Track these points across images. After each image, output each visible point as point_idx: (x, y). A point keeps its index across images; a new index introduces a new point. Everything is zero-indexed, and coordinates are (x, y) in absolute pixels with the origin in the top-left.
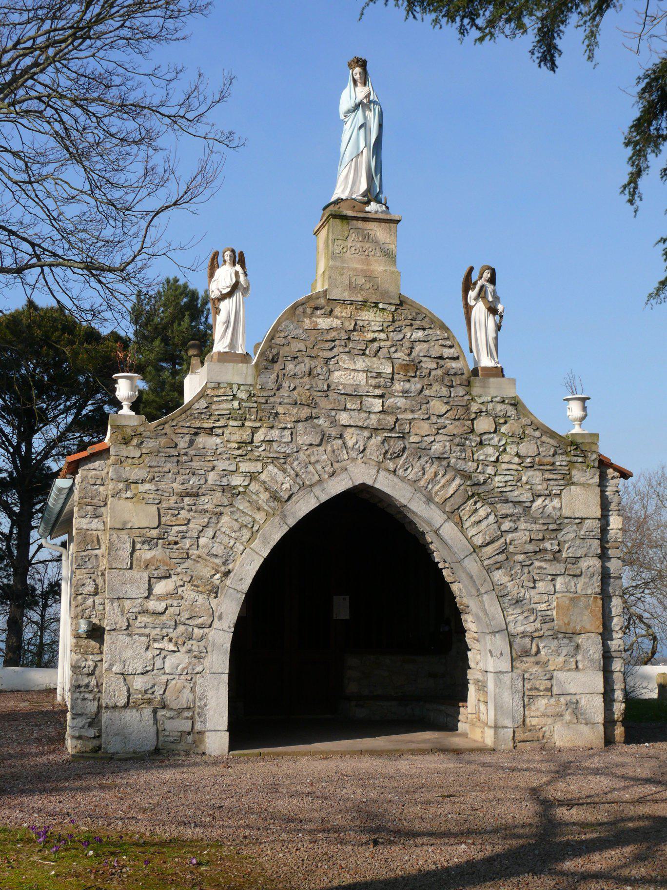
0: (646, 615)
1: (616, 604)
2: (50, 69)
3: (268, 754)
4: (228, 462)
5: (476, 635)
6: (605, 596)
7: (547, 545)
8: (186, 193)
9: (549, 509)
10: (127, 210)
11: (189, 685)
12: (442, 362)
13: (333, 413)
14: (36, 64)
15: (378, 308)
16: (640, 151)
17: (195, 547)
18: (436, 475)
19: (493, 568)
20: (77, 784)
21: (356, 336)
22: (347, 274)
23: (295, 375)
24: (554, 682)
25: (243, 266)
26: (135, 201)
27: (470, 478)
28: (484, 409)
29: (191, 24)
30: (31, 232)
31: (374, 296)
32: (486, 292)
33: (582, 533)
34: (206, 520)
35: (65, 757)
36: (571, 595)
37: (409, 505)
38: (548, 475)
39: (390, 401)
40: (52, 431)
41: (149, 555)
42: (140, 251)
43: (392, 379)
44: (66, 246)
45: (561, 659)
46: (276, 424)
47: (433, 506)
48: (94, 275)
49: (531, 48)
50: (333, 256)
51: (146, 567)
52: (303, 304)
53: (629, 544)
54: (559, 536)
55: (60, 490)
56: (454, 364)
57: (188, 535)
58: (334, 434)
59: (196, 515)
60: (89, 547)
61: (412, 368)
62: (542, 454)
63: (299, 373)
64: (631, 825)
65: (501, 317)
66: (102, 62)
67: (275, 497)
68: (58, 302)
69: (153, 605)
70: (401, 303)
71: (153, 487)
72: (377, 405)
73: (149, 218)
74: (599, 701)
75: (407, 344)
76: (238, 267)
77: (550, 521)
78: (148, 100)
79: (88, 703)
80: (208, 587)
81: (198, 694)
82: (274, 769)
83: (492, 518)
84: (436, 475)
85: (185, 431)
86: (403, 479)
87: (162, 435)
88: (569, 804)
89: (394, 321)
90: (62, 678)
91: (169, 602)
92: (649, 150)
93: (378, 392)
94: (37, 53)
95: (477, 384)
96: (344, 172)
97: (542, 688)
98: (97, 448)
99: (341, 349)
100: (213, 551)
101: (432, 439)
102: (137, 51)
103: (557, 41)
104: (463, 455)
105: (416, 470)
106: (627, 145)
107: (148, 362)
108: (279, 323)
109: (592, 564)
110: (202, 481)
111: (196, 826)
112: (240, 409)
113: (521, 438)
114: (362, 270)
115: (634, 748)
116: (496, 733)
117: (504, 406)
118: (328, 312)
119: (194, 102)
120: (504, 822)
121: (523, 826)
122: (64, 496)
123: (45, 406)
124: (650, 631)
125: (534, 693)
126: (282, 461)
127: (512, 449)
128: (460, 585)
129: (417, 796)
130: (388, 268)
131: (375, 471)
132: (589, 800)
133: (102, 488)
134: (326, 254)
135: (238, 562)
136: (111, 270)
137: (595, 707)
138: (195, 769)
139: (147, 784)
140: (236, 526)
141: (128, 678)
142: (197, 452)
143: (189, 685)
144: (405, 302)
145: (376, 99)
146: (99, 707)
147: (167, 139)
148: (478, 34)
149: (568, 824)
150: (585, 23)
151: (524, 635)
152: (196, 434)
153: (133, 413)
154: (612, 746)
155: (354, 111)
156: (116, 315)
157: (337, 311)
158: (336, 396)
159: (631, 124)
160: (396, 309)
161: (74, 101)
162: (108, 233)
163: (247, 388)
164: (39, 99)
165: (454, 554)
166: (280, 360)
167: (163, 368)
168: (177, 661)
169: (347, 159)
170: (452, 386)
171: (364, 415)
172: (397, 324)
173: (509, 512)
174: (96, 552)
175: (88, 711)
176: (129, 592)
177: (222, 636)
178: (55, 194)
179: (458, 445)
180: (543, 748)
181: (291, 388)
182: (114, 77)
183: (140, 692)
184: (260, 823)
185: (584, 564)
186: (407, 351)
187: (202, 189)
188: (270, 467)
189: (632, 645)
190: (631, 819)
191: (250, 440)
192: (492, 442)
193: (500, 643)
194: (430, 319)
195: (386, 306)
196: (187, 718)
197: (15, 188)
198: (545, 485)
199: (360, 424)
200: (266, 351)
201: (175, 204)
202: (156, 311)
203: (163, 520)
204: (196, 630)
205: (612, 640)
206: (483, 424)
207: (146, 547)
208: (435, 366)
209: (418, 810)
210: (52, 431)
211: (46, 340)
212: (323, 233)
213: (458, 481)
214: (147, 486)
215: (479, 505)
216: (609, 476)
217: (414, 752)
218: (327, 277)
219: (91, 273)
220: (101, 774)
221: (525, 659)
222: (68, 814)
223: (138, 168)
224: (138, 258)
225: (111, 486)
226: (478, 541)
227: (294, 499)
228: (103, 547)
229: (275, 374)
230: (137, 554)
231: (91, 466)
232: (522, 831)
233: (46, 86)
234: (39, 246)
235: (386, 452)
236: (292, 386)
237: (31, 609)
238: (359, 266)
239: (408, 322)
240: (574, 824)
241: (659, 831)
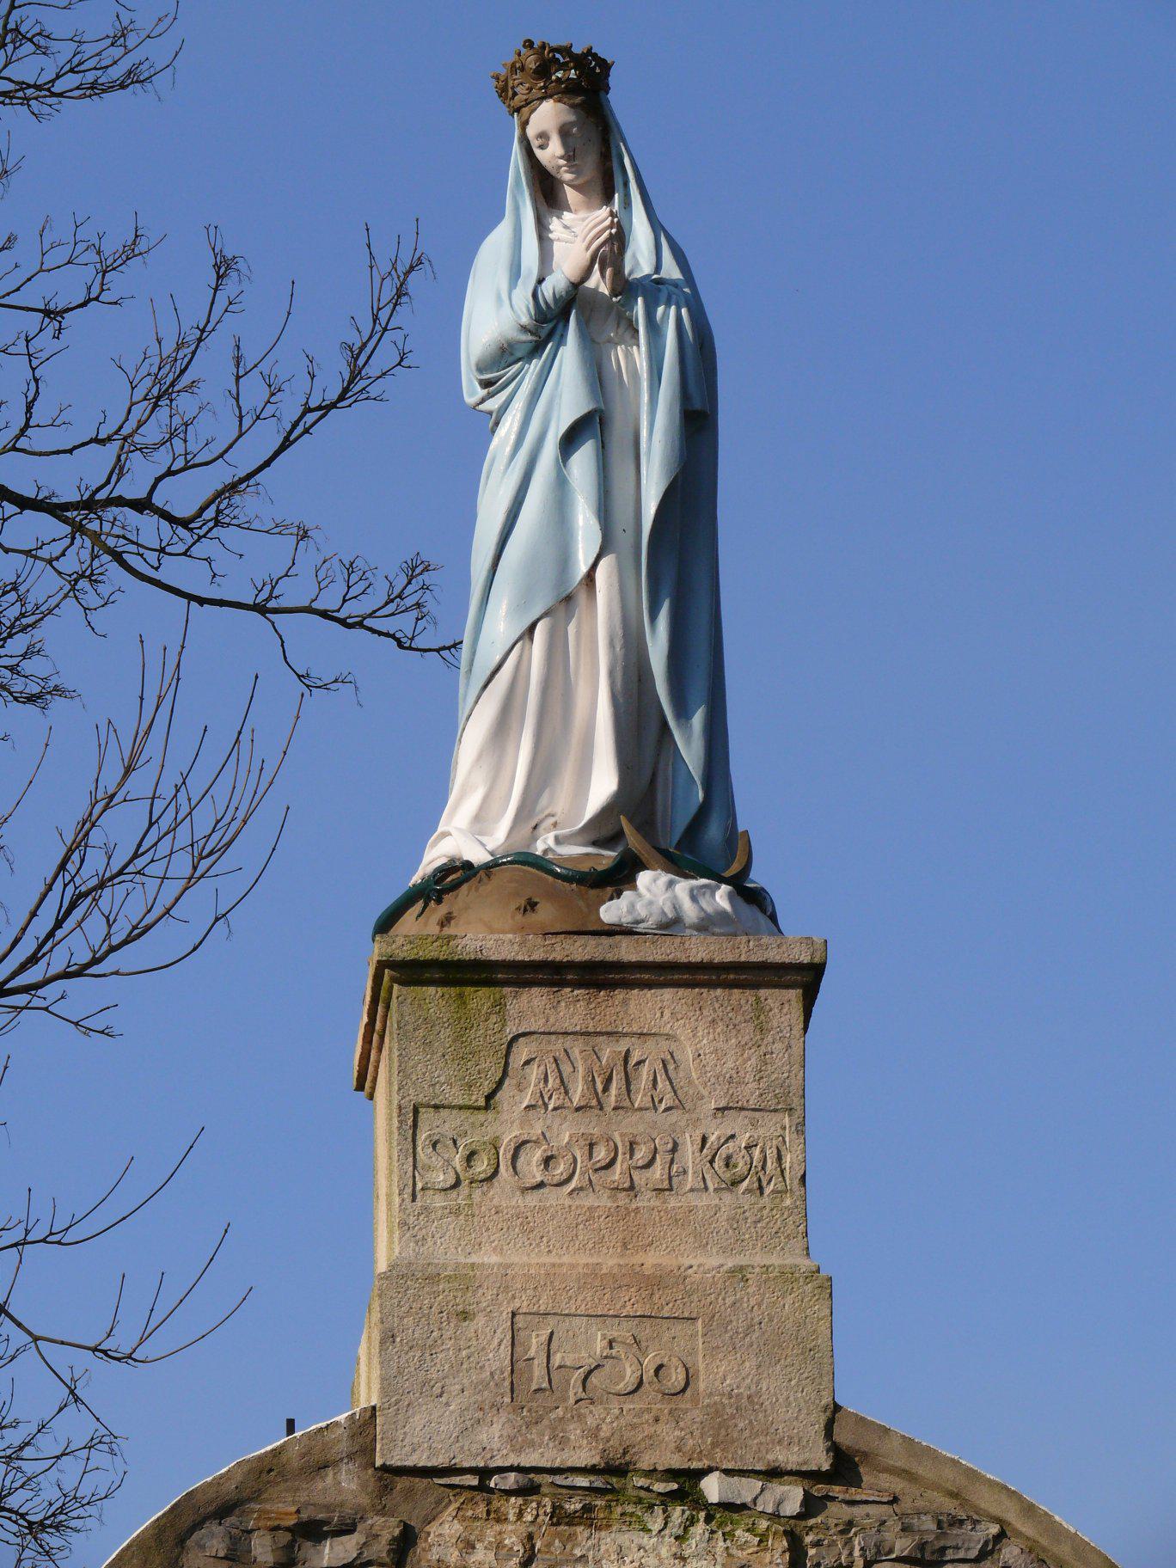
31: (669, 1433)
145: (671, 271)
155: (536, 349)
160: (811, 1506)
195: (746, 1490)
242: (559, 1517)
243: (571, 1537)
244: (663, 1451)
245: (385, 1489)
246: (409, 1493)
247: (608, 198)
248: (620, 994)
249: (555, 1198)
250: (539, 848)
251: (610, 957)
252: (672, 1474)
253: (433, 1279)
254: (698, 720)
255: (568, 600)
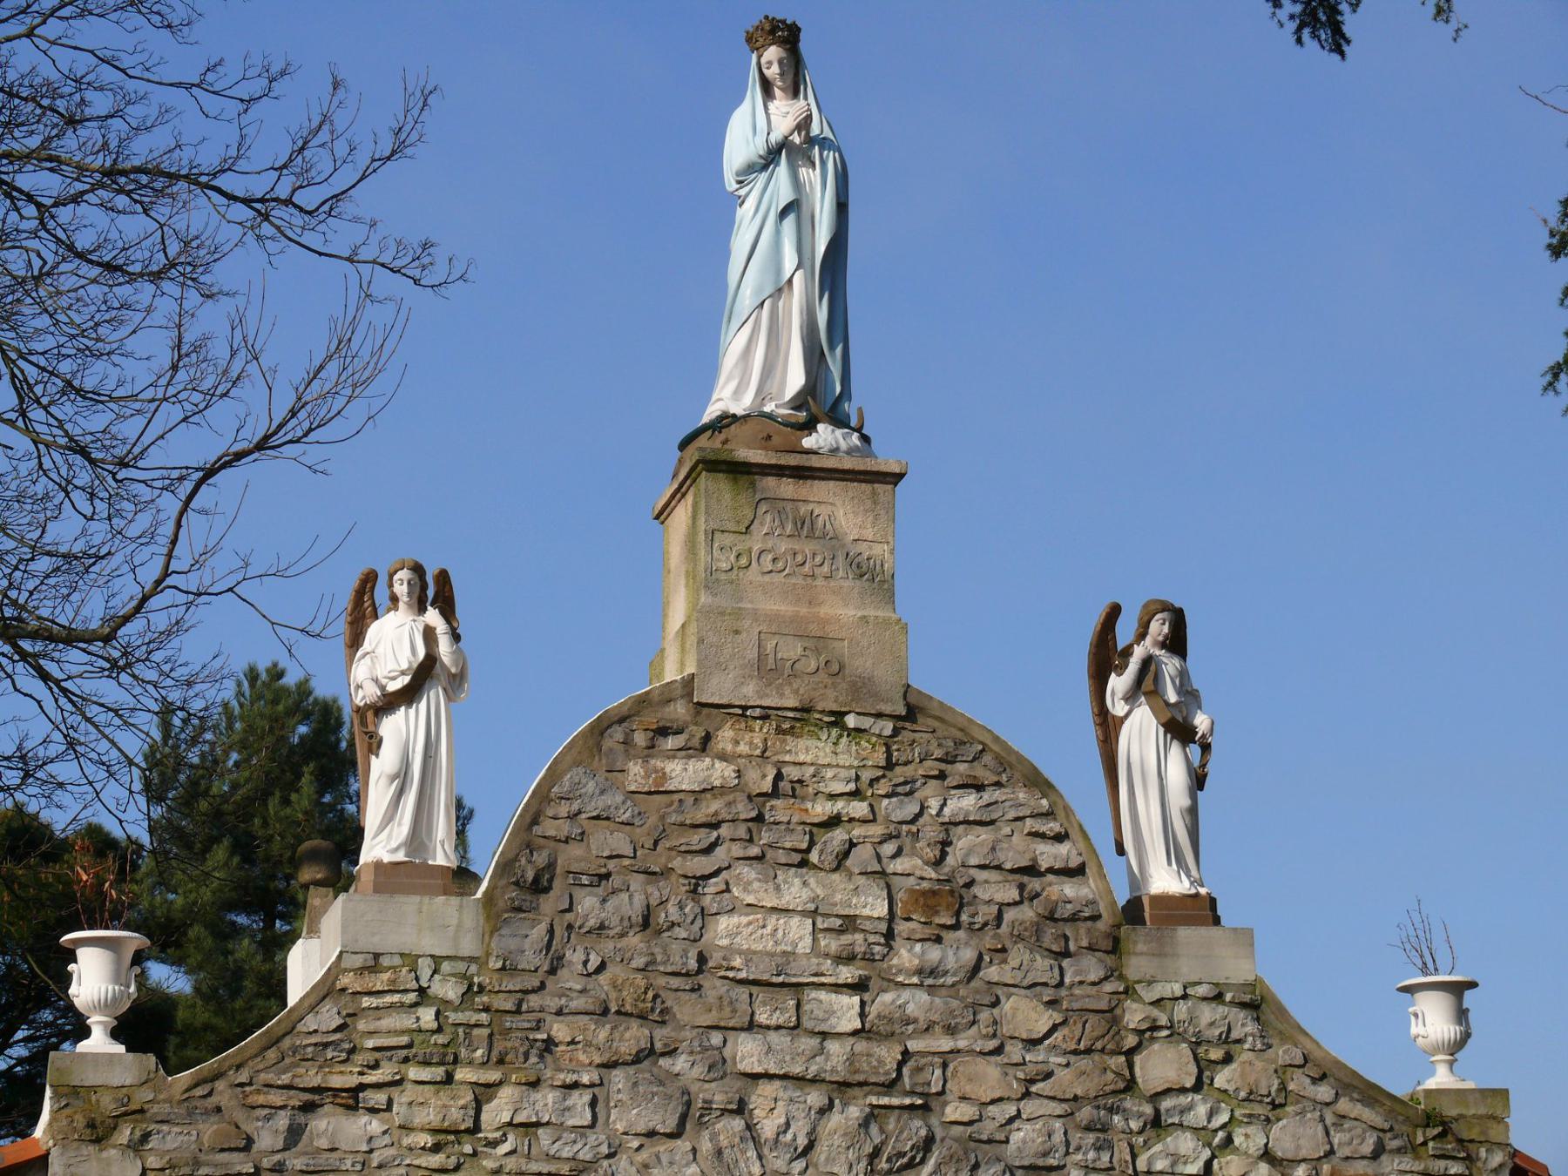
8: (293, 413)
10: (123, 464)
12: (1034, 884)
13: (716, 1038)
15: (844, 727)
21: (779, 810)
23: (602, 927)
25: (448, 612)
26: (146, 440)
28: (1163, 1021)
31: (831, 694)
32: (1158, 678)
39: (885, 1000)
42: (158, 582)
43: (889, 935)
46: (548, 1073)
48: (24, 656)
50: (707, 581)
52: (621, 721)
56: (1070, 889)
61: (945, 902)
62: (1342, 1152)
63: (615, 921)
65: (1206, 748)
66: (55, 51)
72: (845, 1012)
73: (188, 486)
75: (931, 832)
76: (433, 617)
78: (186, 154)
85: (276, 1098)
87: (206, 1112)
89: (890, 765)
93: (847, 974)
95: (1141, 947)
96: (737, 344)
101: (1011, 1110)
102: (156, 19)
104: (1105, 1157)
107: (191, 914)
108: (553, 776)
112: (439, 1030)
113: (1275, 1106)
118: (696, 742)
119: (320, 160)
127: (1249, 1139)
130: (871, 612)
134: (691, 575)
136: (70, 638)
144: (922, 710)
145: (827, 133)
147: (241, 265)
152: (309, 1108)
155: (765, 168)
156: (90, 769)
157: (725, 737)
158: (722, 988)
160: (896, 732)
162: (65, 532)
163: (461, 967)
166: (556, 884)
167: (236, 930)
169: (747, 299)
170: (1066, 954)
171: (808, 1043)
172: (900, 773)
179: (1088, 1129)
181: (592, 967)
182: (90, 95)
186: (931, 853)
187: (339, 402)
191: (469, 1124)
192: (1189, 1119)
194: (997, 757)
195: (866, 723)
199: (797, 1070)
200: (516, 859)
201: (261, 446)
202: (216, 762)
206: (1162, 1066)
208: (1014, 894)
212: (681, 516)
218: (692, 640)
219: (15, 646)
223: (154, 346)
224: (154, 603)
229: (542, 928)
235: (875, 1154)
236: (594, 961)
238: (784, 608)
239: (932, 767)
242: (779, 731)
243: (785, 741)
244: (829, 702)
245: (698, 713)
246: (708, 716)
247: (796, 94)
248: (809, 482)
249: (778, 578)
250: (767, 409)
251: (807, 464)
252: (832, 713)
253: (722, 614)
254: (839, 350)
255: (782, 289)
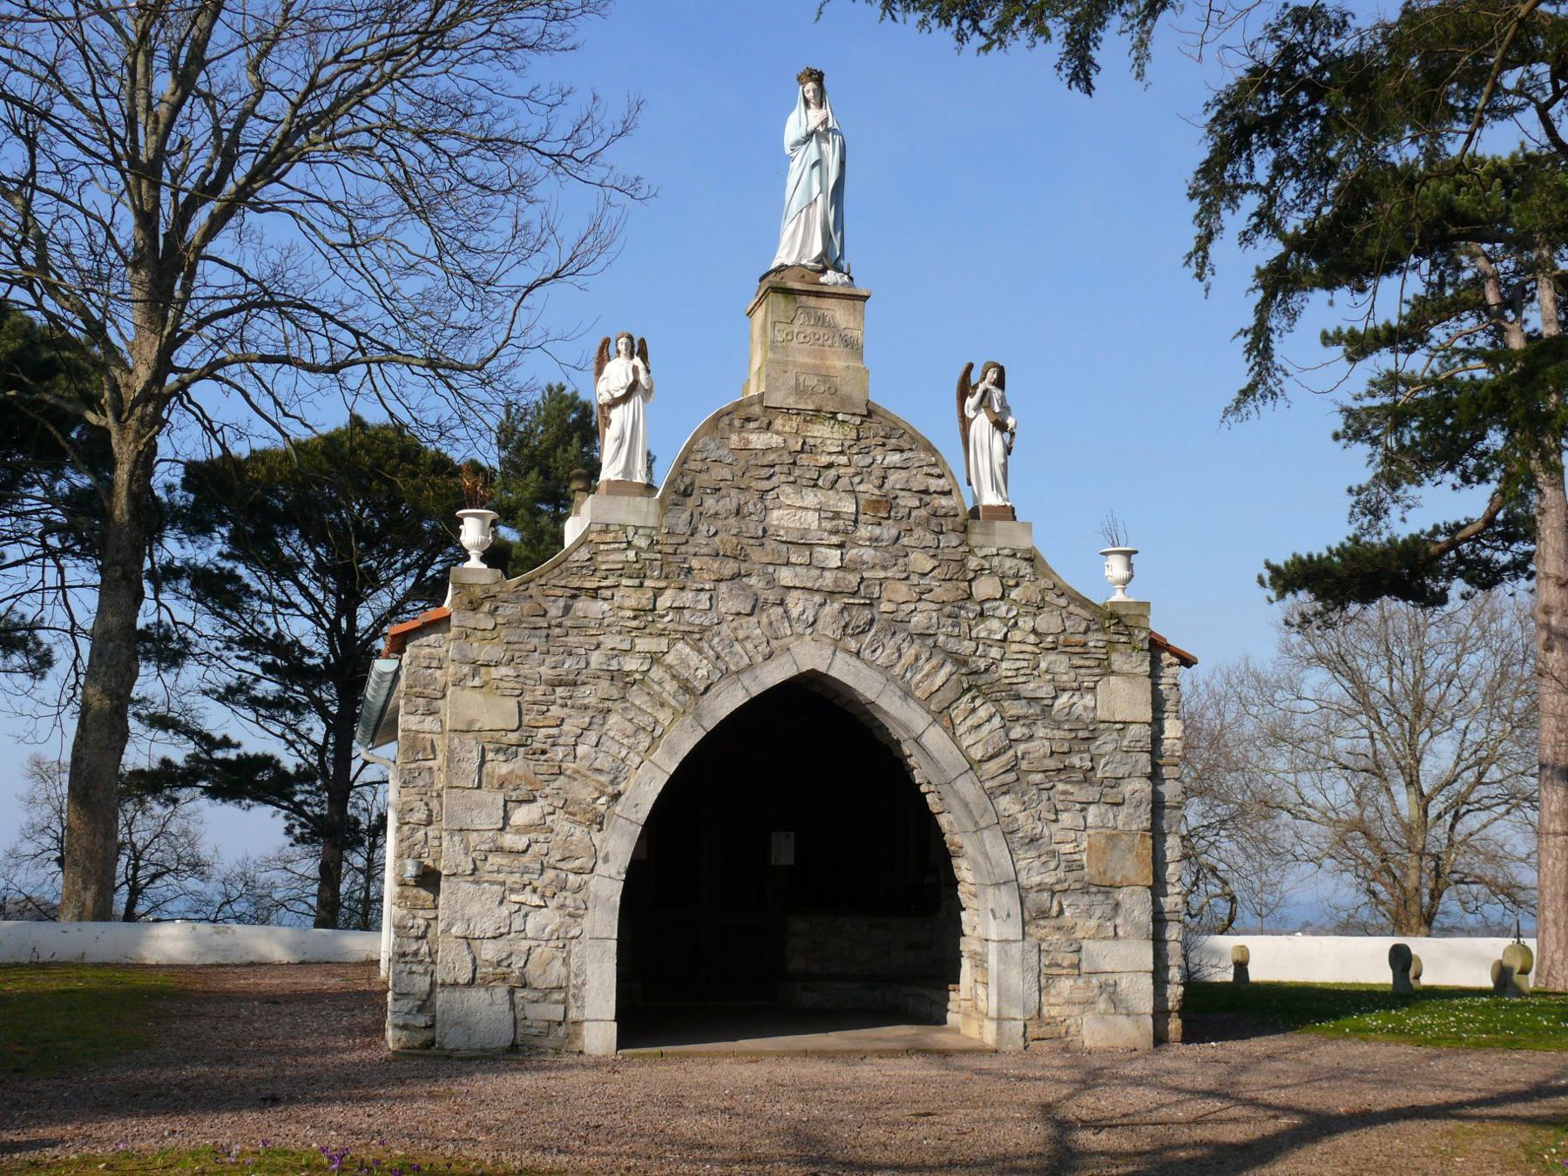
0: (1221, 866)
1: (1173, 847)
2: (386, 89)
3: (672, 1055)
4: (618, 638)
5: (972, 888)
6: (1157, 834)
7: (1076, 760)
9: (1078, 710)
11: (561, 955)
12: (927, 498)
13: (771, 569)
14: (367, 84)
16: (1210, 205)
17: (571, 758)
18: (917, 659)
19: (998, 792)
20: (397, 1091)
21: (804, 459)
22: (792, 371)
24: (1083, 955)
27: (965, 663)
29: (584, 29)
30: (351, 314)
32: (990, 400)
33: (1125, 743)
34: (587, 720)
35: (385, 1054)
36: (1109, 832)
37: (878, 702)
38: (1077, 661)
39: (853, 553)
40: (383, 600)
41: (504, 769)
43: (856, 521)
44: (403, 335)
45: (1093, 922)
47: (912, 703)
49: (1057, 61)
50: (773, 346)
51: (501, 786)
53: (1199, 767)
54: (1092, 748)
55: (381, 675)
56: (944, 501)
57: (561, 741)
58: (771, 598)
59: (573, 712)
60: (420, 756)
61: (884, 506)
64: (1182, 1154)
65: (1012, 434)
66: (458, 80)
67: (686, 687)
68: (391, 414)
69: (509, 840)
70: (870, 414)
71: (512, 672)
72: (833, 558)
73: (520, 295)
74: (1147, 983)
75: (877, 472)
76: (637, 361)
77: (1079, 725)
79: (417, 978)
80: (589, 816)
81: (573, 967)
82: (680, 1076)
83: (996, 721)
84: (917, 659)
85: (559, 592)
86: (870, 664)
88: (1097, 1126)
89: (858, 439)
90: (383, 944)
91: (533, 836)
92: (1223, 205)
93: (835, 540)
94: (368, 68)
97: (1065, 964)
98: (433, 613)
99: (783, 479)
100: (597, 765)
103: (1093, 53)
105: (888, 651)
106: (1192, 197)
107: (520, 504)
108: (694, 440)
109: (1138, 787)
110: (583, 664)
111: (560, 1151)
113: (1039, 608)
114: (814, 366)
115: (1195, 1048)
116: (999, 1028)
117: (1015, 561)
120: (1002, 1150)
121: (1029, 1157)
122: (387, 685)
123: (375, 564)
124: (1227, 890)
125: (1055, 971)
126: (696, 637)
127: (1026, 623)
128: (951, 817)
129: (880, 1114)
131: (830, 652)
132: (1125, 1121)
133: (439, 672)
134: (764, 343)
135: (632, 780)
136: (462, 368)
137: (1140, 992)
138: (566, 1074)
139: (497, 1093)
140: (630, 729)
141: (473, 943)
142: (576, 624)
143: (561, 955)
146: (433, 984)
148: (983, 41)
149: (1093, 1154)
150: (1132, 27)
151: (1041, 888)
152: (574, 597)
153: (485, 566)
154: (1165, 1046)
156: (471, 432)
157: (778, 423)
158: (774, 545)
159: (1197, 168)
161: (419, 135)
162: (460, 316)
164: (369, 130)
165: (943, 771)
167: (541, 512)
168: (544, 920)
169: (794, 208)
170: (941, 533)
171: (816, 572)
172: (863, 443)
173: (1021, 712)
174: (430, 763)
175: (416, 990)
176: (477, 821)
177: (608, 886)
178: (388, 262)
180: (1066, 1049)
182: (475, 102)
183: (491, 964)
184: (654, 1153)
185: (1128, 788)
187: (594, 255)
188: (680, 645)
189: (1201, 908)
190: (1185, 1146)
192: (998, 613)
193: (1007, 900)
195: (848, 418)
196: (557, 1002)
197: (333, 254)
198: (1072, 674)
199: (809, 585)
201: (555, 276)
203: (526, 719)
204: (571, 877)
205: (1166, 895)
206: (986, 587)
207: (501, 757)
209: (880, 1133)
210: (383, 600)
211: (375, 471)
212: (760, 313)
213: (948, 668)
214: (504, 670)
215: (978, 702)
216: (1165, 663)
217: (881, 1054)
218: (763, 375)
220: (433, 1078)
221: (1042, 922)
222: (379, 1133)
223: (504, 226)
224: (502, 352)
225: (452, 669)
226: (977, 753)
227: (713, 690)
228: (440, 757)
229: (688, 514)
230: (488, 767)
231: (424, 640)
232: (1027, 1163)
233: (380, 114)
234: (365, 335)
237: (353, 850)
238: (810, 361)
239: (879, 440)
240: (1102, 1153)
241: (1222, 1163)
